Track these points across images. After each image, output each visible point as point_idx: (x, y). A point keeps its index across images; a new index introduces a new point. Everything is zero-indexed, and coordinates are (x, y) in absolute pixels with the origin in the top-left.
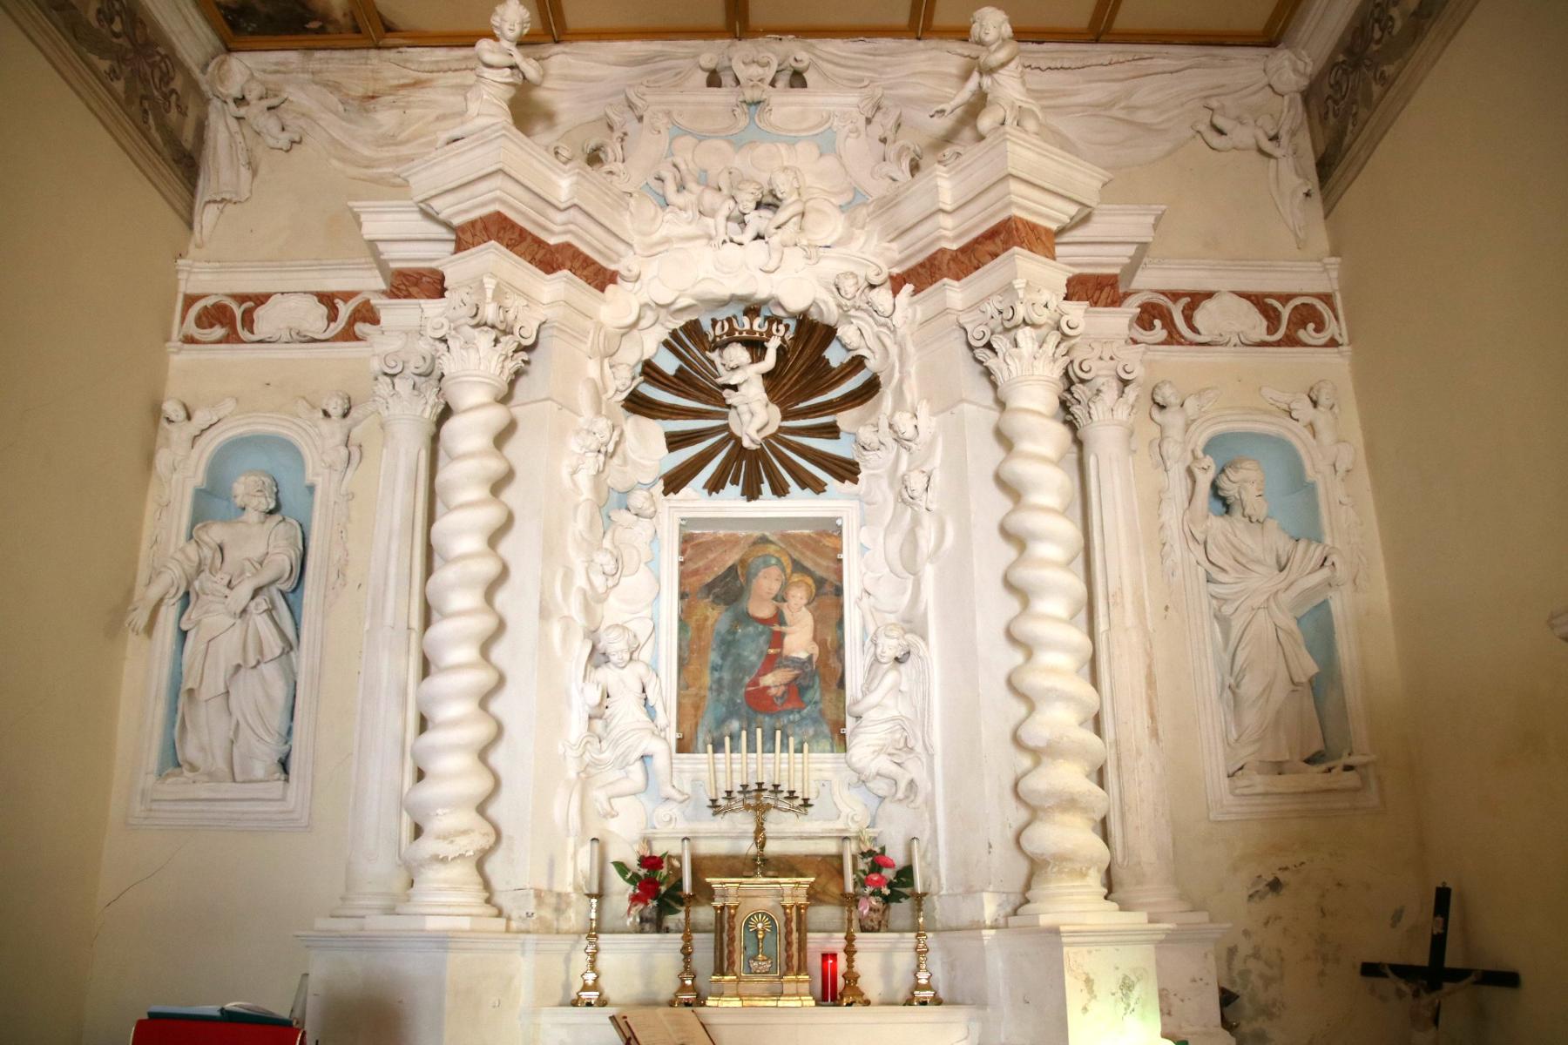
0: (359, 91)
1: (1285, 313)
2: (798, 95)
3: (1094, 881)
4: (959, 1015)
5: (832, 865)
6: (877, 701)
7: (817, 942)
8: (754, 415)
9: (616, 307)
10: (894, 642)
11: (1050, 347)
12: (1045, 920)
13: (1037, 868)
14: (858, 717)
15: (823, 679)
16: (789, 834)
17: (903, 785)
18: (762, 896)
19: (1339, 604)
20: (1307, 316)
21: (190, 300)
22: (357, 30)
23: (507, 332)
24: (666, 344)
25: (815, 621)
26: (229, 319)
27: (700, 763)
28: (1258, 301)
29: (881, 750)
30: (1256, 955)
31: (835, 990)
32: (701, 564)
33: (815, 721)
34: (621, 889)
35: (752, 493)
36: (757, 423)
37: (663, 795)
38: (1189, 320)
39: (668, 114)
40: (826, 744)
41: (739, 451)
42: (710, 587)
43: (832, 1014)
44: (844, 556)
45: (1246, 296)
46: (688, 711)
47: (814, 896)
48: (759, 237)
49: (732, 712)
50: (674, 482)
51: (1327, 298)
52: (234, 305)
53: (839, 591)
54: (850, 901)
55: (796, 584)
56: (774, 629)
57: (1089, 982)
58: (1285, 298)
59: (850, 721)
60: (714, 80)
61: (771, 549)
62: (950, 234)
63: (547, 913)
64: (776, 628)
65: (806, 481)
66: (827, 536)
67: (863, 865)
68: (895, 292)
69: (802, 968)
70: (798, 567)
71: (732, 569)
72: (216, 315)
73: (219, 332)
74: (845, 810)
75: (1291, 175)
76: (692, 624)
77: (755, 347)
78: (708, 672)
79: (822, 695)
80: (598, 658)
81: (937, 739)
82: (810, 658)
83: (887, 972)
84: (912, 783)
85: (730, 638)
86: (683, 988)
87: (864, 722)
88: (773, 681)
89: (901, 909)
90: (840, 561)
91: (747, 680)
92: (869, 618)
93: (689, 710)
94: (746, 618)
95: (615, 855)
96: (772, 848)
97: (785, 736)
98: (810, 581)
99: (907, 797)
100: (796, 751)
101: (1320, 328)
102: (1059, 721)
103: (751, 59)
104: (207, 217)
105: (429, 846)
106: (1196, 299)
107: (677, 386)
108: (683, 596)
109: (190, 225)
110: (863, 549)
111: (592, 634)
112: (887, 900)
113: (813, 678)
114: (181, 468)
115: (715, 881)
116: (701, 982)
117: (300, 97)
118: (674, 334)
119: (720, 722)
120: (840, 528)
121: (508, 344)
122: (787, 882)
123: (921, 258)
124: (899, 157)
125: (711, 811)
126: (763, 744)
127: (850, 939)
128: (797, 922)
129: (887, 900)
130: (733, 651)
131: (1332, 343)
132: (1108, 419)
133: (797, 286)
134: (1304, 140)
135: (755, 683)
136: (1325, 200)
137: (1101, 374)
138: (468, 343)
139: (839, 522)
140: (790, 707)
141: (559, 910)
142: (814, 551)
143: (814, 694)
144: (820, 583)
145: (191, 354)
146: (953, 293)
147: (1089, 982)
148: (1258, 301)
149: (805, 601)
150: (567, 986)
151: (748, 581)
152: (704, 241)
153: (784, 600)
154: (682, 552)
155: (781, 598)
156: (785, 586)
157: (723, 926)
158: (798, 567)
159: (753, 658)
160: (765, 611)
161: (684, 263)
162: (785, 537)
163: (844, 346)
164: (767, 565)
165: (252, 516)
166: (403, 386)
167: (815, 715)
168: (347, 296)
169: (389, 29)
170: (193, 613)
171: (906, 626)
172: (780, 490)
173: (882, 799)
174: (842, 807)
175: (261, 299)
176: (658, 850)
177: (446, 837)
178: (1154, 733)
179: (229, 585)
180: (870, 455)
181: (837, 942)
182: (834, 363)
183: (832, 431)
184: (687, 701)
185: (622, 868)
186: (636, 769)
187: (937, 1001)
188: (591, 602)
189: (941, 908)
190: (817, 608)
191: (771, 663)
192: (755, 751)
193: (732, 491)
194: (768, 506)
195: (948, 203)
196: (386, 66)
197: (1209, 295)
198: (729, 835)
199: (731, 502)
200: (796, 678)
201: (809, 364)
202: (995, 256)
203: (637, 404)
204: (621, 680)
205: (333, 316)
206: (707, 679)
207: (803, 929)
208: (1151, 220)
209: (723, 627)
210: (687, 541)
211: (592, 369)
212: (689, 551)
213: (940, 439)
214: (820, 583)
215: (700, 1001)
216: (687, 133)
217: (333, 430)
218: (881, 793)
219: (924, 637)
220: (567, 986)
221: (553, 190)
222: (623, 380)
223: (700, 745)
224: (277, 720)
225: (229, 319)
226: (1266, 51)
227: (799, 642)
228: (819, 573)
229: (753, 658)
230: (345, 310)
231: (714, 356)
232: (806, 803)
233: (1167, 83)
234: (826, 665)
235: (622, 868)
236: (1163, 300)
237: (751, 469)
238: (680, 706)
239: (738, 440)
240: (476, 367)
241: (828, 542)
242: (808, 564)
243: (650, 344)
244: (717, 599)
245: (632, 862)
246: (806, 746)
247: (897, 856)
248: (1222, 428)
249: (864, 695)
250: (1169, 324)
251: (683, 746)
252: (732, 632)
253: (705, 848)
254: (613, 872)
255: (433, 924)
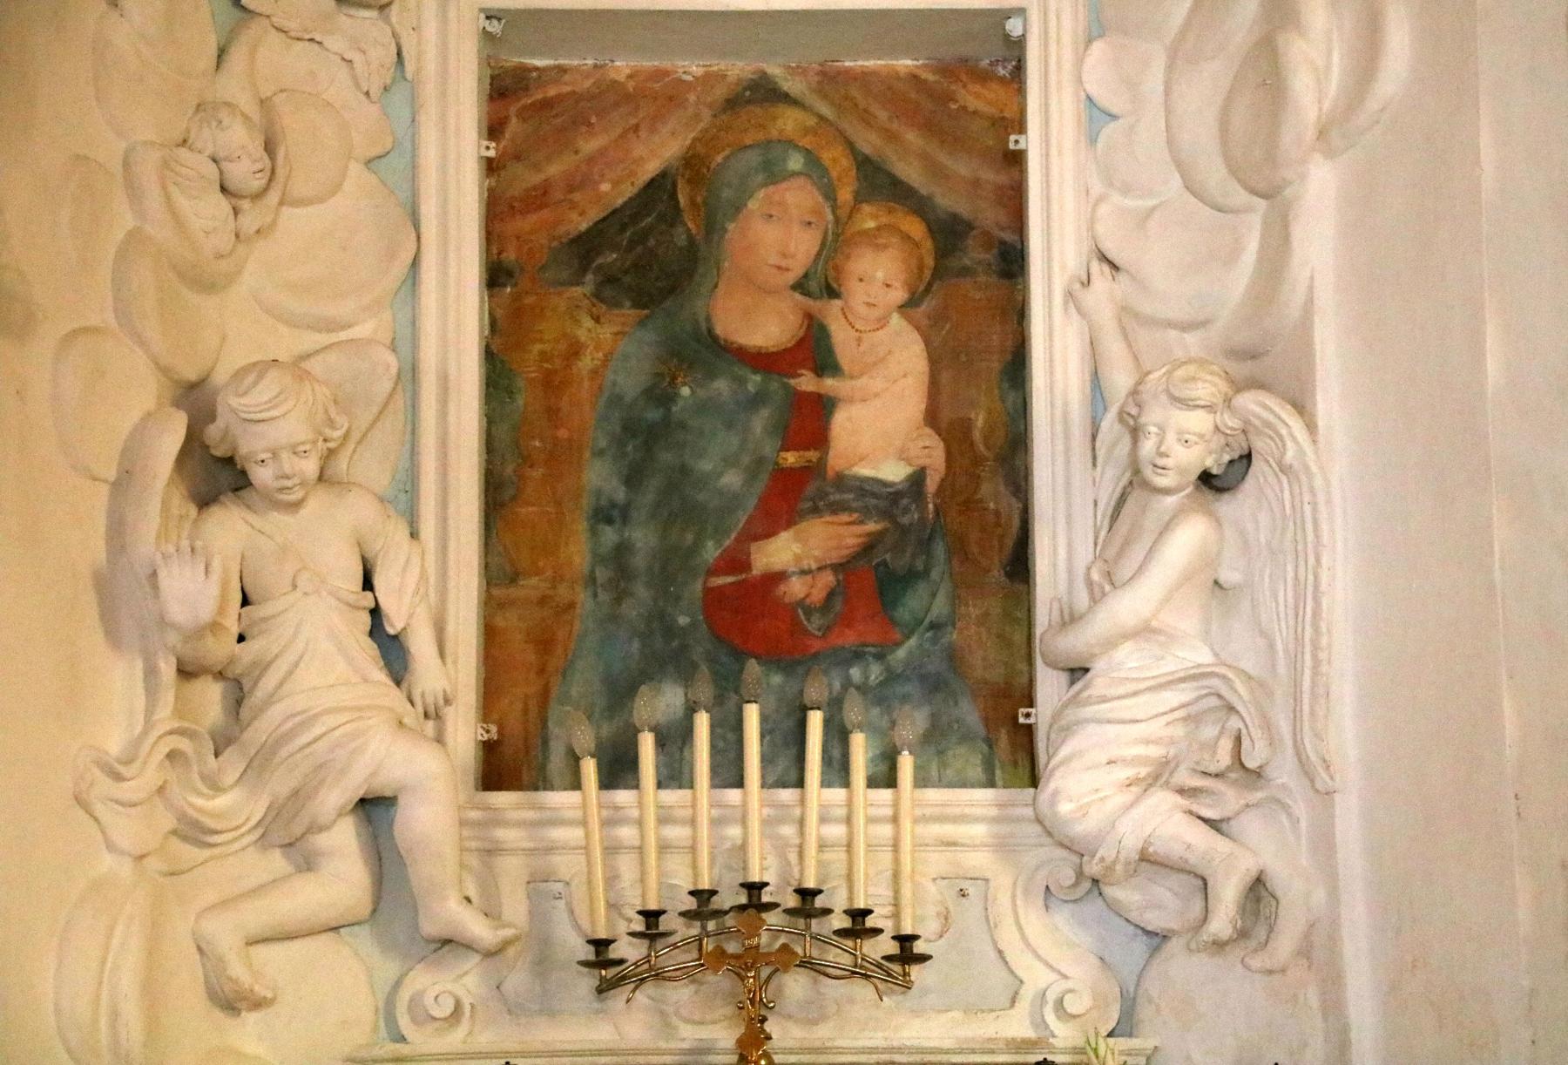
6: (1138, 637)
10: (1198, 422)
14: (1078, 672)
15: (959, 549)
17: (1228, 894)
25: (934, 361)
29: (1158, 775)
32: (554, 170)
33: (934, 686)
37: (430, 928)
40: (969, 760)
42: (584, 248)
44: (1032, 142)
46: (520, 660)
53: (1012, 262)
55: (870, 238)
59: (1049, 686)
61: (789, 121)
64: (806, 382)
70: (878, 182)
71: (660, 186)
74: (1036, 977)
76: (529, 365)
78: (582, 526)
79: (955, 600)
81: (1345, 735)
82: (917, 480)
84: (1258, 890)
85: (654, 415)
87: (1098, 683)
88: (795, 554)
90: (1017, 160)
91: (711, 552)
92: (1114, 348)
93: (520, 650)
94: (706, 351)
97: (838, 734)
98: (915, 228)
99: (1243, 934)
100: (872, 783)
108: (496, 276)
110: (1095, 115)
113: (926, 545)
120: (1017, 47)
125: (586, 982)
126: (766, 760)
130: (666, 457)
135: (736, 562)
139: (1014, 27)
140: (849, 639)
142: (929, 127)
143: (928, 600)
144: (949, 234)
149: (899, 295)
151: (713, 228)
153: (833, 293)
154: (493, 130)
155: (821, 283)
156: (837, 244)
158: (878, 182)
159: (732, 480)
160: (766, 327)
162: (831, 80)
163: (1034, 799)
164: (773, 174)
167: (935, 665)
171: (1241, 370)
173: (1158, 939)
174: (1022, 962)
184: (502, 431)
190: (938, 318)
191: (793, 493)
192: (739, 783)
200: (869, 547)
206: (578, 551)
209: (630, 379)
210: (505, 91)
212: (514, 126)
214: (949, 234)
218: (1154, 920)
219: (1302, 407)
223: (557, 761)
227: (882, 426)
228: (948, 201)
229: (732, 480)
232: (907, 952)
234: (970, 505)
238: (490, 635)
241: (974, 98)
242: (910, 172)
244: (611, 289)
246: (906, 763)
249: (1097, 597)
251: (501, 768)
252: (660, 393)
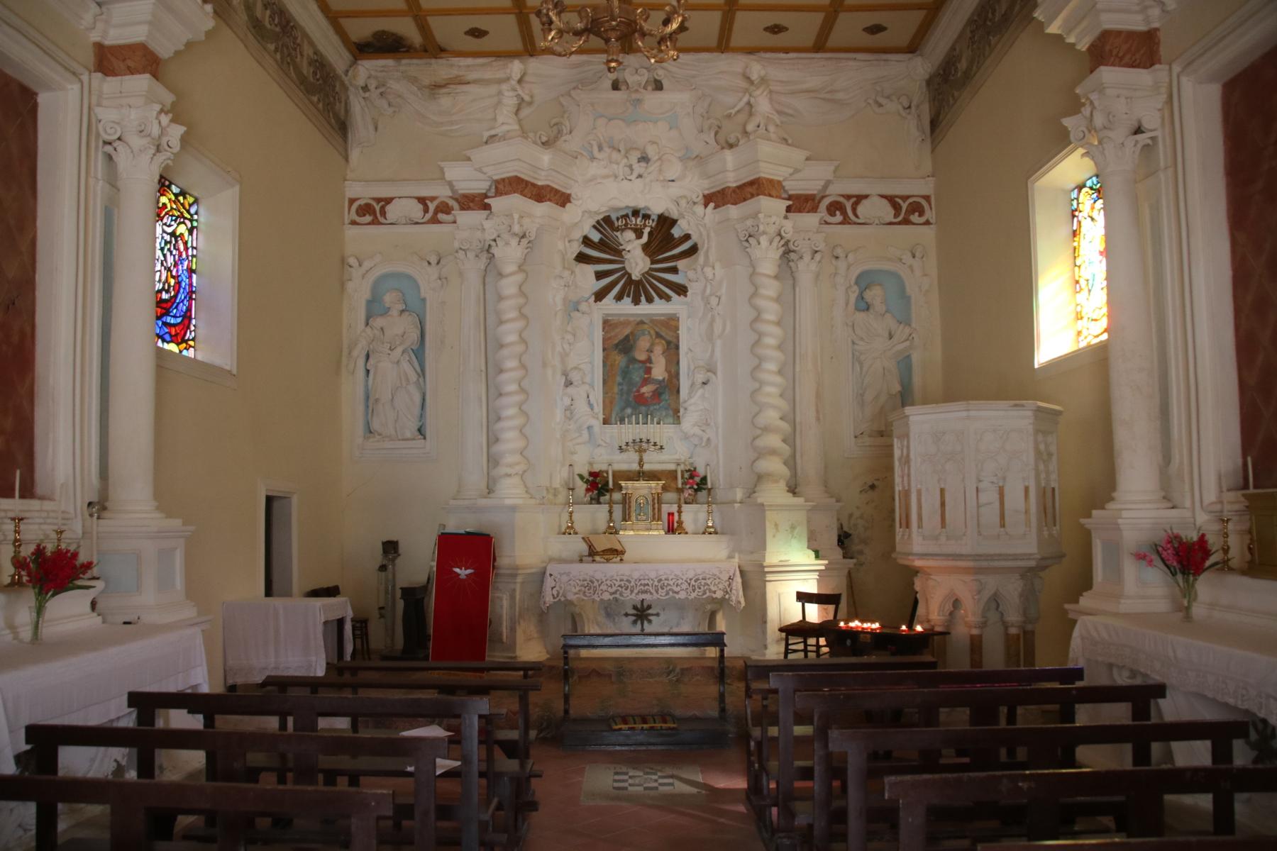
0: (427, 82)
1: (905, 206)
2: (658, 94)
3: (782, 485)
4: (724, 538)
5: (672, 475)
6: (694, 402)
7: (666, 509)
8: (637, 262)
9: (570, 214)
11: (775, 244)
12: (760, 500)
13: (760, 478)
16: (654, 461)
18: (641, 489)
19: (916, 357)
20: (917, 208)
21: (352, 201)
22: (426, 51)
23: (523, 236)
24: (594, 227)
26: (373, 211)
27: (613, 429)
28: (891, 199)
30: (861, 517)
31: (673, 528)
34: (581, 487)
35: (636, 301)
36: (638, 269)
38: (854, 210)
39: (592, 105)
41: (630, 281)
42: (617, 345)
43: (671, 536)
45: (882, 196)
46: (608, 404)
47: (665, 488)
48: (640, 176)
49: (627, 404)
50: (600, 296)
51: (927, 198)
52: (374, 204)
53: (677, 347)
54: (680, 491)
56: (647, 365)
57: (776, 525)
58: (905, 198)
59: (682, 410)
60: (616, 86)
62: (732, 179)
63: (551, 497)
65: (663, 296)
66: (671, 323)
67: (686, 475)
68: (706, 206)
69: (659, 519)
70: (658, 335)
71: (627, 336)
72: (366, 210)
73: (368, 218)
75: (913, 129)
77: (639, 234)
80: (569, 383)
83: (695, 521)
86: (609, 527)
89: (702, 495)
94: (633, 360)
95: (578, 470)
96: (647, 467)
101: (921, 214)
102: (771, 416)
103: (635, 68)
104: (354, 155)
105: (502, 470)
106: (860, 198)
107: (600, 247)
108: (604, 350)
109: (347, 159)
110: (689, 329)
111: (565, 374)
112: (696, 491)
114: (359, 290)
115: (623, 483)
116: (617, 526)
117: (395, 86)
118: (598, 222)
119: (623, 409)
121: (524, 241)
122: (653, 484)
123: (719, 188)
124: (710, 128)
127: (680, 507)
128: (658, 501)
129: (696, 491)
131: (927, 223)
132: (806, 269)
133: (658, 204)
134: (926, 108)
136: (932, 142)
137: (803, 246)
138: (507, 244)
141: (555, 495)
143: (665, 396)
144: (669, 343)
145: (355, 230)
146: (733, 211)
147: (776, 525)
148: (891, 199)
150: (560, 526)
152: (612, 179)
155: (650, 351)
156: (652, 345)
157: (625, 501)
158: (658, 335)
160: (641, 356)
161: (602, 190)
162: (652, 321)
165: (395, 312)
166: (471, 255)
168: (433, 199)
169: (442, 50)
170: (372, 361)
172: (650, 300)
175: (388, 201)
176: (596, 468)
177: (510, 466)
178: (818, 419)
179: (391, 349)
180: (694, 284)
181: (674, 508)
182: (676, 236)
183: (674, 270)
185: (581, 477)
186: (585, 434)
187: (716, 533)
188: (564, 356)
189: (720, 494)
191: (646, 382)
193: (627, 300)
194: (644, 309)
195: (731, 169)
196: (442, 69)
197: (866, 197)
198: (628, 462)
199: (626, 307)
201: (664, 237)
202: (753, 196)
203: (582, 258)
204: (579, 392)
205: (426, 210)
206: (616, 390)
207: (660, 502)
208: (832, 168)
211: (560, 246)
213: (725, 285)
214: (669, 343)
215: (616, 532)
216: (602, 116)
217: (433, 272)
219: (715, 373)
220: (560, 526)
221: (542, 165)
222: (577, 248)
224: (417, 411)
225: (373, 211)
226: (910, 55)
227: (659, 372)
228: (668, 338)
230: (432, 206)
231: (618, 234)
232: (662, 448)
233: (852, 76)
235: (581, 477)
236: (842, 199)
237: (636, 290)
239: (630, 275)
240: (510, 253)
241: (673, 323)
243: (587, 229)
245: (586, 475)
247: (701, 471)
248: (866, 268)
250: (844, 213)
251: (606, 422)
252: (627, 367)
253: (617, 467)
254: (577, 479)
255: (508, 502)
